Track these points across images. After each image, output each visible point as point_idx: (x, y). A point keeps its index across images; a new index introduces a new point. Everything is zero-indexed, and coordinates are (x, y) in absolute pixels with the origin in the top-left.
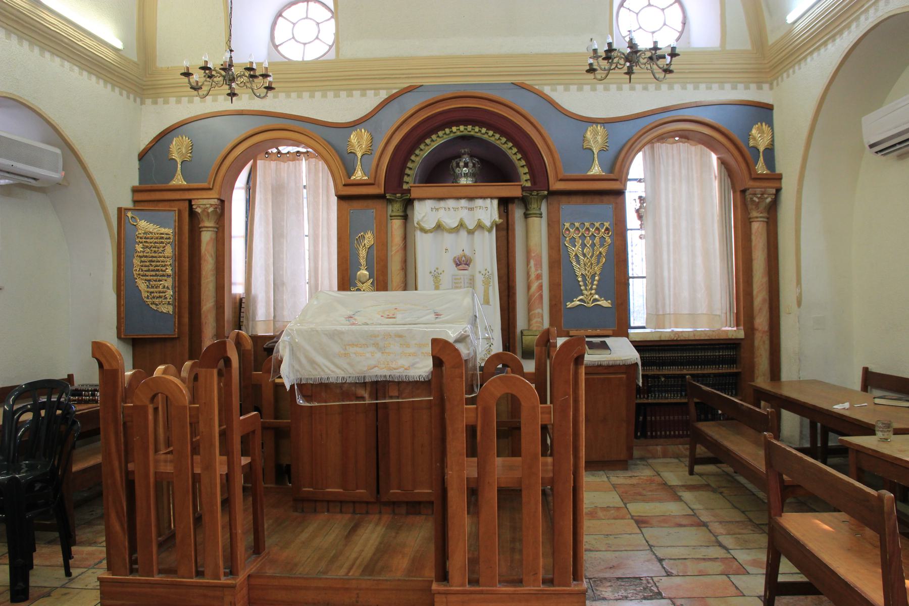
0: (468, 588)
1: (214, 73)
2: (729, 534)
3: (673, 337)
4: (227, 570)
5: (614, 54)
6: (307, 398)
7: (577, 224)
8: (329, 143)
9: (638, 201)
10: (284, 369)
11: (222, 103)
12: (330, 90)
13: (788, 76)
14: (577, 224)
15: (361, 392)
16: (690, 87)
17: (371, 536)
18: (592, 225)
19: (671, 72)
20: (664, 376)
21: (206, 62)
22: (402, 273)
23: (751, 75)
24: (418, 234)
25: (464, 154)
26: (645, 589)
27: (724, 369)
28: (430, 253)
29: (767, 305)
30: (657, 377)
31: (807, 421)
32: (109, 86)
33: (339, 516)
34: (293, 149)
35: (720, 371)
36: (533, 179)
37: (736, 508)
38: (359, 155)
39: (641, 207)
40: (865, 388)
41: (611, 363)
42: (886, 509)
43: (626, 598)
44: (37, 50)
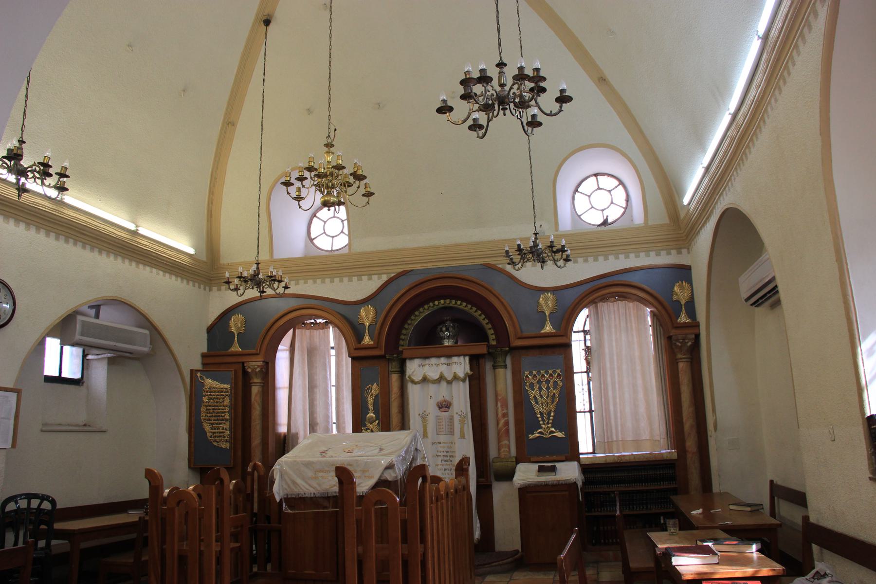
6: (290, 507)
7: (534, 372)
14: (534, 372)
15: (326, 504)
16: (622, 256)
27: (665, 485)
32: (185, 281)
36: (497, 339)
38: (367, 324)
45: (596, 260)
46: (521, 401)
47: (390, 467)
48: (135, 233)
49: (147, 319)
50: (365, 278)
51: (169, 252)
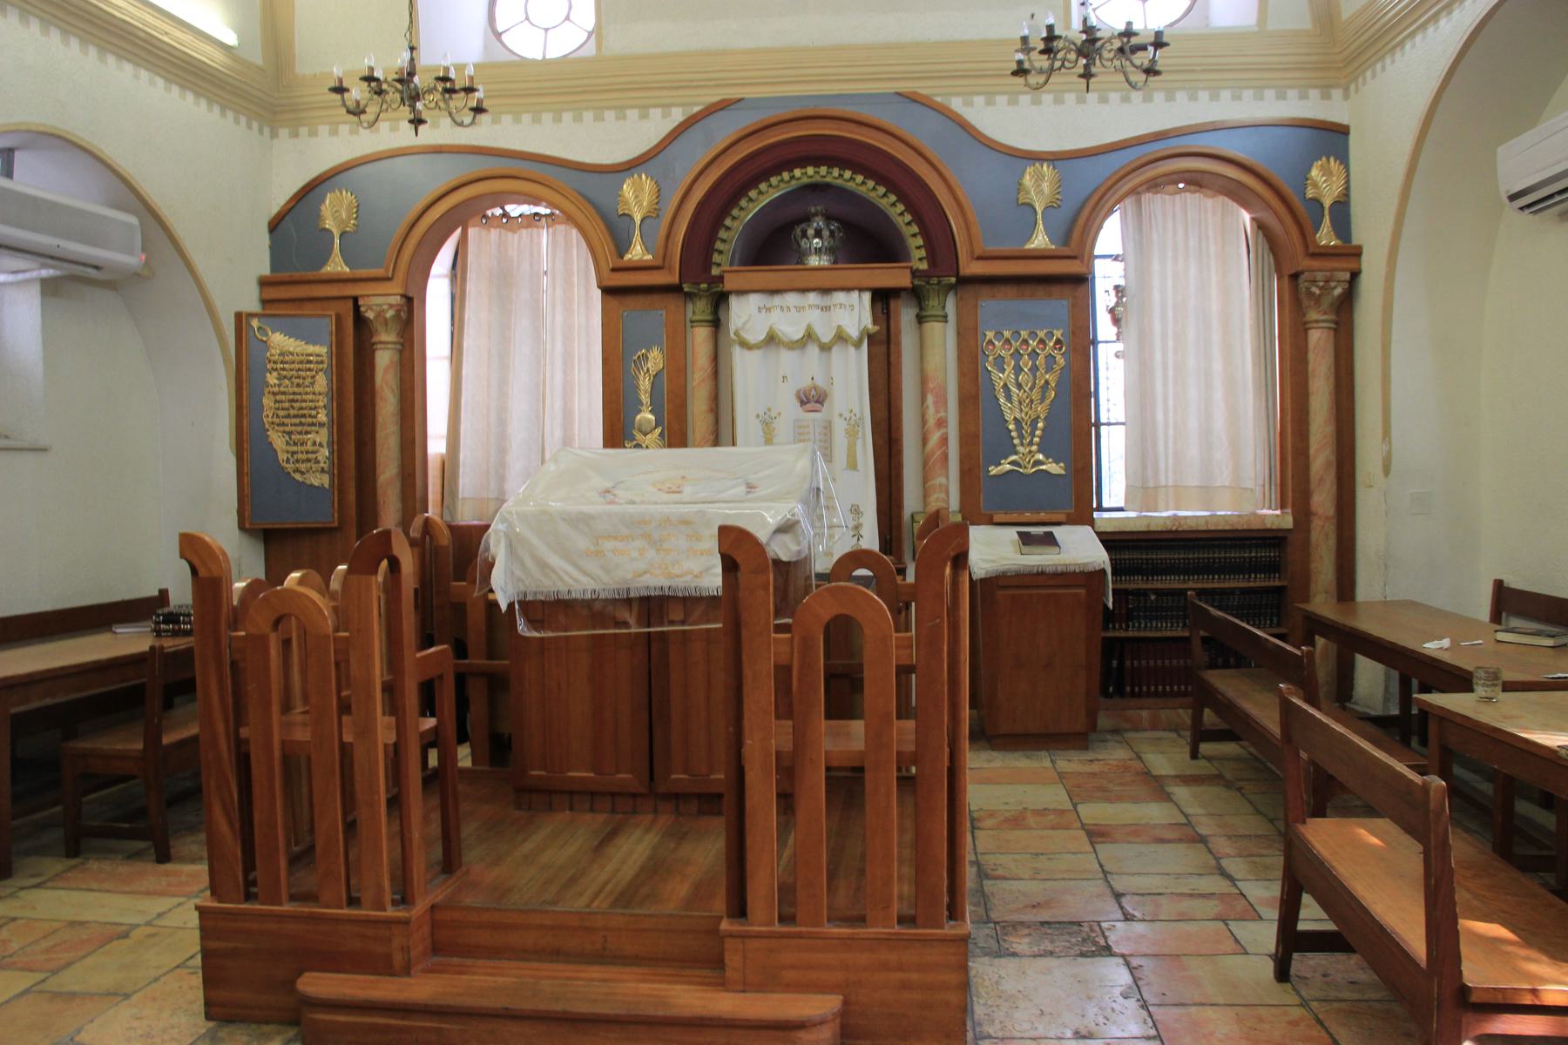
0: (778, 928)
1: (385, 86)
2: (1240, 856)
3: (1170, 526)
4: (398, 897)
5: (1057, 44)
6: (533, 623)
7: (1007, 334)
8: (589, 200)
9: (1113, 293)
10: (498, 578)
11: (404, 136)
12: (587, 109)
13: (1374, 76)
14: (1007, 334)
16: (1204, 96)
17: (635, 848)
18: (1033, 335)
19: (1157, 73)
20: (1156, 591)
21: (371, 69)
22: (711, 417)
23: (1298, 74)
24: (737, 351)
25: (816, 214)
26: (1084, 940)
28: (756, 382)
30: (1139, 593)
31: (1395, 674)
32: (216, 109)
33: (588, 817)
34: (527, 209)
36: (932, 257)
37: (1259, 812)
38: (638, 218)
39: (1117, 304)
40: (1496, 617)
41: (1060, 569)
42: (1432, 805)
43: (1052, 953)
46: (975, 394)
50: (633, 114)
51: (178, 34)
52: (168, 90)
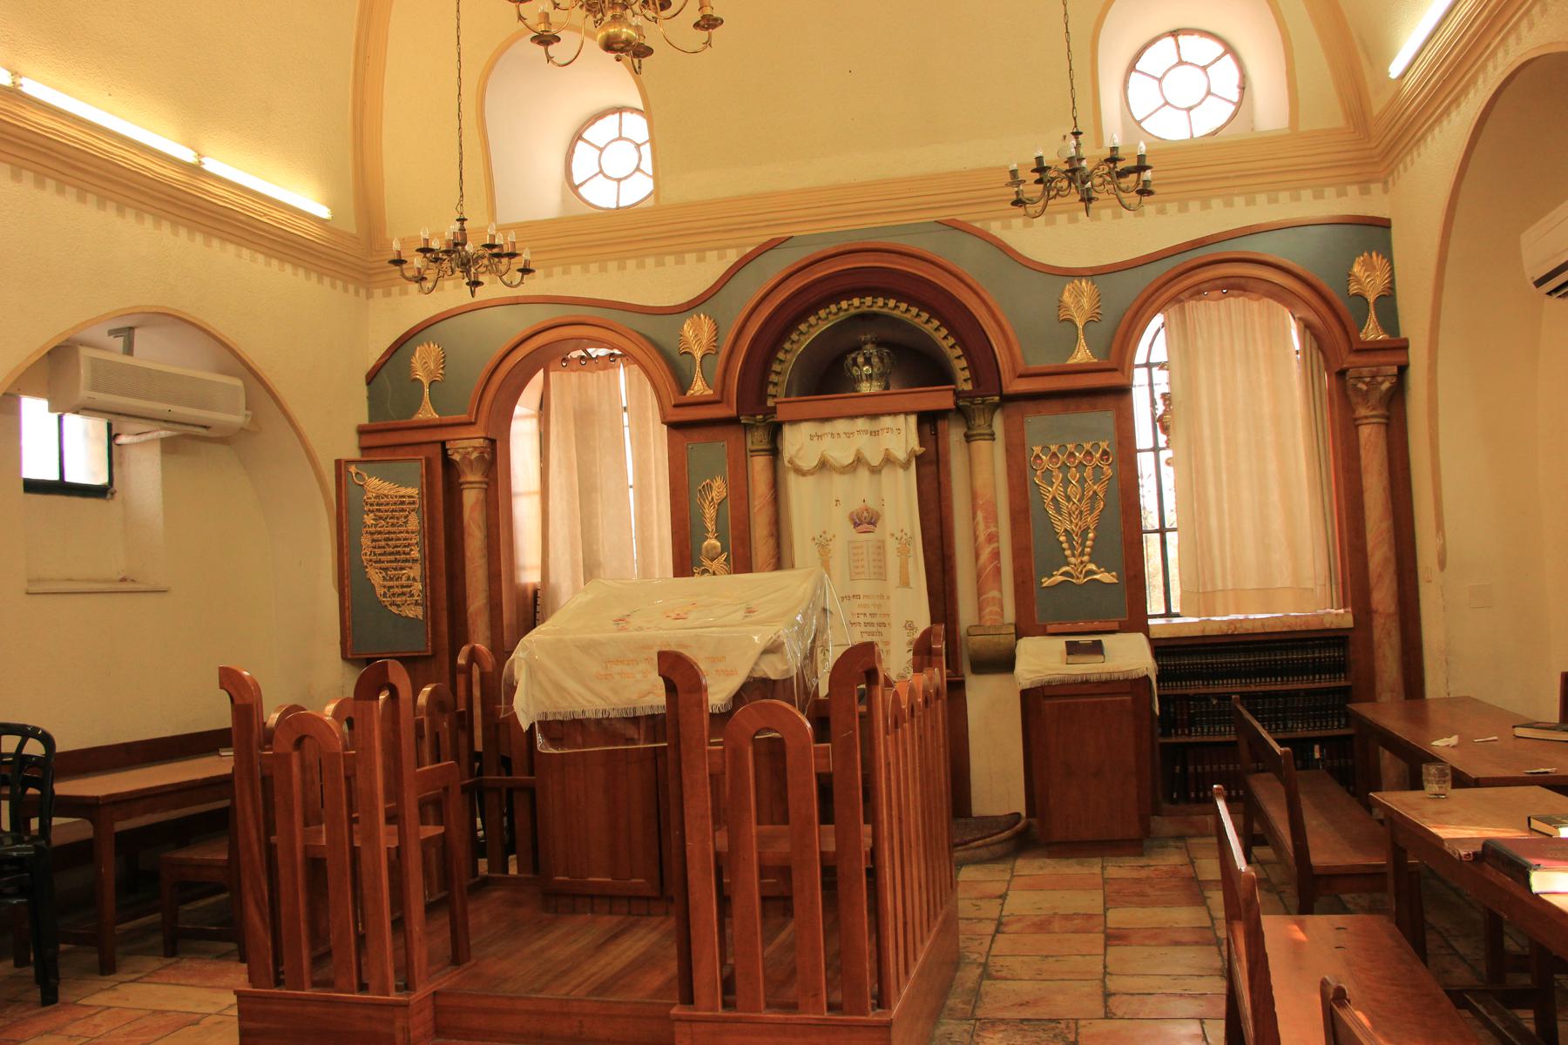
6: (552, 740)
7: (1054, 448)
13: (1406, 169)
14: (1054, 448)
15: (631, 732)
18: (1079, 447)
19: (1150, 193)
20: (1214, 695)
22: (772, 542)
25: (865, 343)
27: (1324, 682)
28: (812, 508)
29: (1392, 568)
32: (314, 277)
33: (607, 918)
34: (603, 352)
35: (1317, 685)
36: (975, 378)
38: (698, 355)
41: (1104, 677)
44: (199, 238)
45: (1183, 209)
46: (1023, 511)
47: (773, 649)
48: (196, 170)
49: (243, 362)
51: (276, 214)
52: (268, 264)
